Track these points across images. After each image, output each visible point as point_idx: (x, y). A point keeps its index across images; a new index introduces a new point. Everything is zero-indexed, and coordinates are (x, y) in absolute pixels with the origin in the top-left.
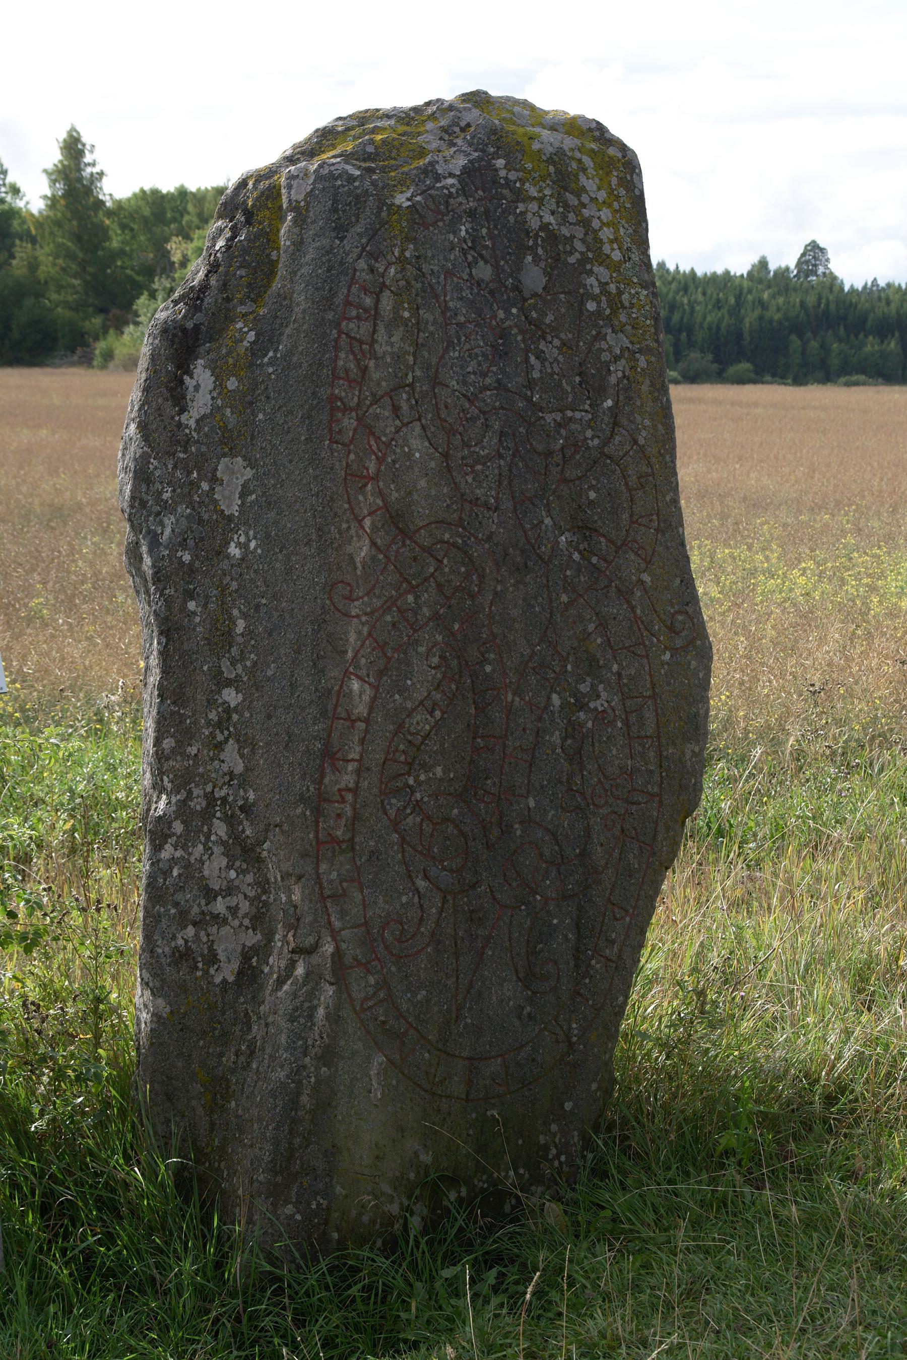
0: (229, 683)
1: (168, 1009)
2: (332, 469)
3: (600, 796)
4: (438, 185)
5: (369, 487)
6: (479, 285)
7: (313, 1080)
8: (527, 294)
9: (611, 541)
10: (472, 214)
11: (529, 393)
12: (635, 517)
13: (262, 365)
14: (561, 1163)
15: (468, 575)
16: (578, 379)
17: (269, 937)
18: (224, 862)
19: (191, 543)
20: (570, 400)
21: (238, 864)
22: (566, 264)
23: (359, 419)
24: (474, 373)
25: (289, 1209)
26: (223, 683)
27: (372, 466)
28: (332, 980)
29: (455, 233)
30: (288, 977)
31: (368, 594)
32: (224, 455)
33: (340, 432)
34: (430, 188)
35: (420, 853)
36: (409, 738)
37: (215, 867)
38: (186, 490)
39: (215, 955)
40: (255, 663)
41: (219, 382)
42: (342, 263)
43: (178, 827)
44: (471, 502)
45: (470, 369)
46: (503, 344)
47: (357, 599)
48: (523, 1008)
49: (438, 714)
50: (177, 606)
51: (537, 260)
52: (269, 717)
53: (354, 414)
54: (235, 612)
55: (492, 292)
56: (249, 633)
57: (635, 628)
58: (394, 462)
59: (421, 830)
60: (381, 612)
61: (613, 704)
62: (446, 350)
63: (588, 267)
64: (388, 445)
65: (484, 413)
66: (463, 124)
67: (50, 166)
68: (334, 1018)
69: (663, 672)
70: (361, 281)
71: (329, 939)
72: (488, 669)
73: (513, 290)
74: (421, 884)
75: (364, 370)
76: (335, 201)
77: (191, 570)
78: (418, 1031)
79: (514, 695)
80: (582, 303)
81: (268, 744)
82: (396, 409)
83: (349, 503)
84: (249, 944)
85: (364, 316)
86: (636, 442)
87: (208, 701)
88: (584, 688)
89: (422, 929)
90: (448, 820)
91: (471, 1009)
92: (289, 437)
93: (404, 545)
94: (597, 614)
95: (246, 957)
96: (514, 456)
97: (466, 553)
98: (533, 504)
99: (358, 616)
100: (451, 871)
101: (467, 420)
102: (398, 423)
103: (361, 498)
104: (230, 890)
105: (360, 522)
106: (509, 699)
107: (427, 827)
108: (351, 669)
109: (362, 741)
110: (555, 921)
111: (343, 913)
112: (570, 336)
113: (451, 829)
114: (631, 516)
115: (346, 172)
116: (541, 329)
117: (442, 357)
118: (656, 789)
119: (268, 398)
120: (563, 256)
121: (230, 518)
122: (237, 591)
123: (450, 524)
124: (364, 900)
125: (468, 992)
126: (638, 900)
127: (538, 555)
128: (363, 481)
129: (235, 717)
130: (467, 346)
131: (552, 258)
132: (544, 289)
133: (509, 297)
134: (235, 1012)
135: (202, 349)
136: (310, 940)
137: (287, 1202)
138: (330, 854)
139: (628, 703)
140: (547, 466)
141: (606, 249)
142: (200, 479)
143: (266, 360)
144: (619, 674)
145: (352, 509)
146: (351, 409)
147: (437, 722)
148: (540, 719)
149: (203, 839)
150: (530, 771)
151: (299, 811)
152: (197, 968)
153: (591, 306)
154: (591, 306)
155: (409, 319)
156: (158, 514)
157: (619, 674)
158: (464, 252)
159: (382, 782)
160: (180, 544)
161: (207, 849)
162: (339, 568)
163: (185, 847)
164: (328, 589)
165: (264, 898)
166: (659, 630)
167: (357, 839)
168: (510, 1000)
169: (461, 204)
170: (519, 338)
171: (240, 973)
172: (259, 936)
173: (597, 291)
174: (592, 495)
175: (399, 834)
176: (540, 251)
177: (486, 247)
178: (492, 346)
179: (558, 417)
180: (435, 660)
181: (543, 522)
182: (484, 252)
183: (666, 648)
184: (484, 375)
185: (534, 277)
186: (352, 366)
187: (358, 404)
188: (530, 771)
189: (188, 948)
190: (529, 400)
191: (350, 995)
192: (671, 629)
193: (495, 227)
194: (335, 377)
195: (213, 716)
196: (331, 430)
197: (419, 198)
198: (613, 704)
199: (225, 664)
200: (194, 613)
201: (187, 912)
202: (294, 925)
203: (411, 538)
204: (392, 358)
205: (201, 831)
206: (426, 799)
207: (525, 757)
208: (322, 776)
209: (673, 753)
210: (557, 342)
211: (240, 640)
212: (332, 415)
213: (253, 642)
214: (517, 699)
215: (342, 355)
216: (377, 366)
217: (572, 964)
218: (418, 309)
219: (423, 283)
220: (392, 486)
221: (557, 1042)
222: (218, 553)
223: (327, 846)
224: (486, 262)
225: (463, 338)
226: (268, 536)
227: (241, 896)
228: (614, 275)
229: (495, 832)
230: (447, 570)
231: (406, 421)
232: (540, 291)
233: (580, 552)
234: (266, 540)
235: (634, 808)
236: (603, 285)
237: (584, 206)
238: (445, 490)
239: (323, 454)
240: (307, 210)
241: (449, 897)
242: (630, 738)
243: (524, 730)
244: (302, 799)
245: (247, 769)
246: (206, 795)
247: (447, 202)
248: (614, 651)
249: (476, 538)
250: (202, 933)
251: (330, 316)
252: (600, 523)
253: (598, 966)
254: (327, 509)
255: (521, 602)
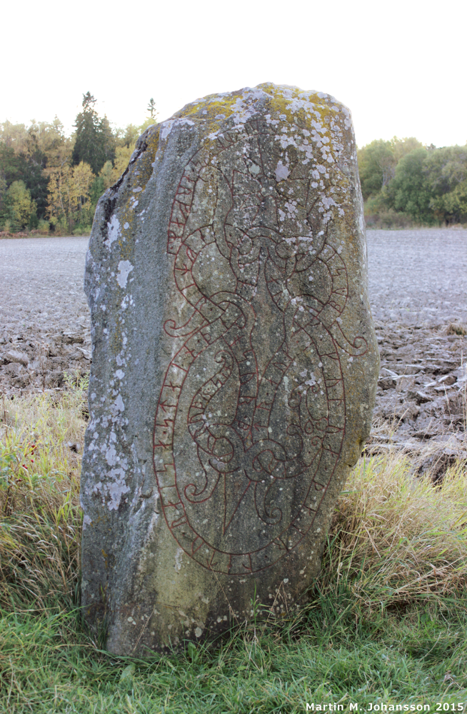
0: (119, 368)
1: (91, 521)
2: (167, 266)
3: (309, 428)
4: (233, 128)
5: (187, 274)
6: (252, 176)
7: (145, 558)
8: (278, 180)
9: (320, 301)
10: (250, 142)
11: (277, 228)
12: (335, 289)
13: (139, 217)
14: (280, 608)
15: (239, 317)
16: (306, 221)
17: (133, 489)
18: (115, 452)
19: (106, 301)
20: (300, 231)
21: (120, 454)
22: (301, 165)
23: (183, 242)
24: (247, 219)
25: (130, 619)
26: (116, 367)
27: (189, 264)
28: (157, 511)
29: (240, 151)
30: (139, 508)
31: (184, 326)
32: (121, 259)
33: (172, 248)
34: (229, 129)
35: (208, 452)
36: (204, 396)
37: (111, 456)
38: (105, 276)
39: (110, 497)
40: (130, 359)
41: (122, 224)
42: (178, 167)
43: (96, 436)
44: (242, 282)
45: (245, 217)
46: (264, 205)
47: (178, 328)
48: (261, 531)
49: (219, 385)
50: (100, 331)
51: (284, 163)
52: (135, 384)
53: (180, 239)
54: (123, 334)
55: (259, 179)
56: (129, 344)
57: (332, 344)
58: (201, 262)
59: (208, 441)
60: (191, 335)
61: (319, 382)
62: (232, 208)
63: (314, 166)
64: (197, 254)
65: (252, 238)
66: (253, 99)
67: (383, 139)
68: (158, 530)
69: (348, 367)
70: (187, 175)
71: (157, 492)
72: (248, 363)
73: (271, 178)
74: (207, 467)
75: (187, 218)
76: (180, 138)
77: (106, 314)
78: (203, 539)
79: (262, 376)
80: (309, 184)
81: (133, 397)
82: (203, 237)
83: (176, 282)
84: (124, 492)
85: (188, 192)
86: (336, 252)
87: (110, 376)
88: (303, 374)
89: (207, 489)
90: (224, 437)
91: (232, 530)
92: (149, 250)
93: (206, 302)
94: (311, 338)
95: (123, 498)
96: (268, 259)
97: (238, 307)
98: (278, 283)
99: (178, 336)
100: (224, 462)
101: (242, 242)
102: (204, 243)
103: (182, 279)
104: (117, 466)
105: (181, 291)
106: (260, 379)
107: (212, 440)
108: (173, 362)
109: (178, 397)
110: (281, 489)
111: (165, 480)
112: (302, 200)
113: (225, 441)
114: (332, 289)
115: (186, 124)
116: (285, 197)
117: (230, 211)
118: (342, 426)
119: (141, 232)
120: (299, 161)
121: (122, 290)
122: (124, 324)
123: (230, 292)
124: (176, 474)
125: (231, 521)
126: (330, 480)
127: (279, 308)
128: (183, 272)
129: (121, 384)
130: (244, 206)
131: (293, 162)
132: (288, 177)
133: (268, 182)
134: (118, 524)
135: (115, 210)
136: (148, 492)
137: (129, 615)
138: (159, 451)
139: (327, 382)
140: (286, 264)
141: (324, 157)
142: (111, 271)
143: (141, 214)
144: (323, 369)
145: (177, 285)
146: (179, 237)
147: (218, 389)
148: (277, 389)
149: (106, 441)
150: (270, 414)
151: (145, 429)
152: (102, 502)
153: (314, 185)
154: (314, 185)
155: (212, 193)
156: (94, 287)
157: (323, 369)
158: (245, 160)
159: (189, 417)
160: (102, 302)
161: (108, 446)
162: (169, 313)
163: (98, 445)
164: (163, 323)
165: (131, 470)
166: (347, 346)
167: (174, 444)
168: (254, 526)
169: (244, 137)
170: (273, 201)
171: (120, 506)
172: (129, 489)
173: (318, 177)
174: (311, 278)
175: (196, 442)
176: (287, 159)
177: (257, 158)
178: (258, 205)
179: (294, 240)
180: (219, 359)
181: (282, 292)
182: (256, 160)
183: (350, 355)
184: (253, 220)
185: (282, 171)
186: (180, 216)
187: (183, 235)
188: (270, 414)
189: (99, 493)
190: (277, 232)
191: (166, 519)
192: (354, 346)
193: (263, 148)
194: (171, 221)
195: (112, 383)
196: (168, 247)
197: (222, 135)
198: (319, 382)
199: (118, 358)
200: (106, 334)
201: (99, 476)
202: (142, 484)
203: (209, 299)
204: (202, 212)
205: (105, 438)
206: (212, 426)
207: (267, 407)
208: (157, 413)
209: (352, 408)
210: (295, 203)
211: (125, 347)
212: (169, 240)
213: (130, 348)
214: (264, 379)
215: (175, 211)
216: (193, 216)
217: (290, 511)
218: (217, 188)
219: (221, 175)
220: (199, 274)
221: (280, 549)
222: (117, 306)
223: (158, 447)
224: (257, 164)
225: (242, 202)
226: (138, 298)
227: (122, 469)
228: (328, 169)
229: (249, 444)
230: (228, 315)
231: (208, 242)
232: (286, 178)
233: (304, 307)
234: (137, 299)
235: (329, 435)
236: (322, 176)
237: (313, 136)
238: (228, 276)
239: (164, 259)
240: (167, 143)
241: (222, 474)
242: (328, 400)
243: (268, 394)
244: (147, 424)
245: (126, 409)
246: (108, 421)
247: (237, 136)
248: (320, 356)
249: (245, 299)
250: (105, 486)
251: (170, 192)
252: (314, 292)
253: (305, 513)
254: (165, 285)
255: (268, 331)
